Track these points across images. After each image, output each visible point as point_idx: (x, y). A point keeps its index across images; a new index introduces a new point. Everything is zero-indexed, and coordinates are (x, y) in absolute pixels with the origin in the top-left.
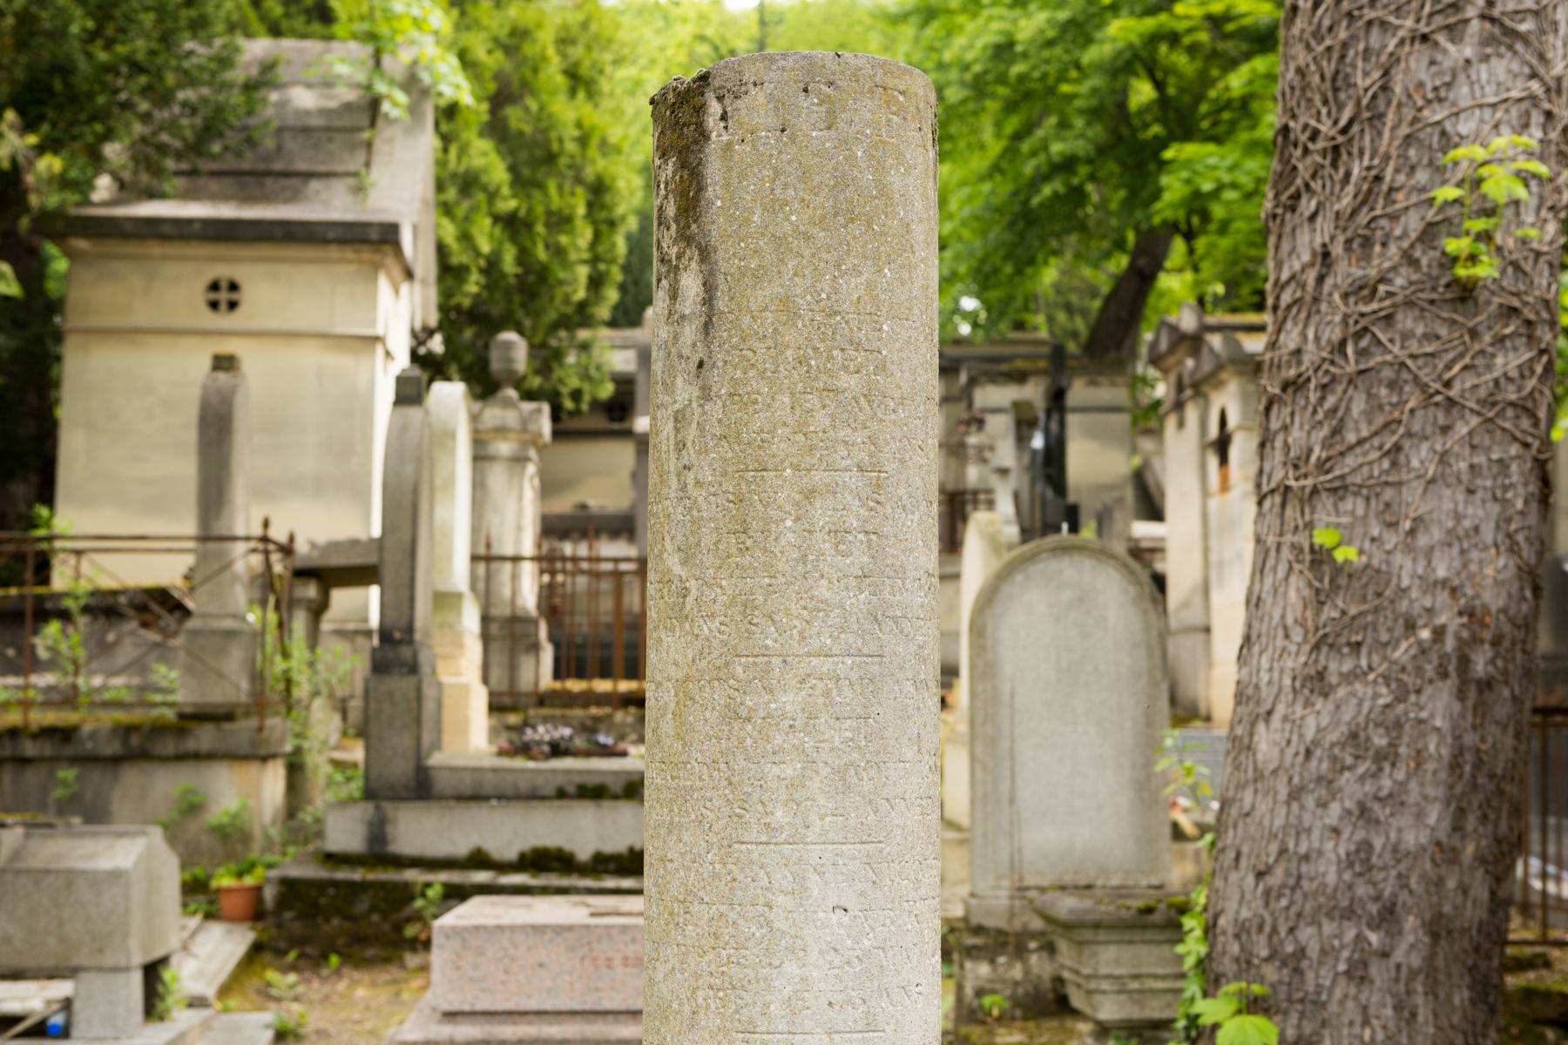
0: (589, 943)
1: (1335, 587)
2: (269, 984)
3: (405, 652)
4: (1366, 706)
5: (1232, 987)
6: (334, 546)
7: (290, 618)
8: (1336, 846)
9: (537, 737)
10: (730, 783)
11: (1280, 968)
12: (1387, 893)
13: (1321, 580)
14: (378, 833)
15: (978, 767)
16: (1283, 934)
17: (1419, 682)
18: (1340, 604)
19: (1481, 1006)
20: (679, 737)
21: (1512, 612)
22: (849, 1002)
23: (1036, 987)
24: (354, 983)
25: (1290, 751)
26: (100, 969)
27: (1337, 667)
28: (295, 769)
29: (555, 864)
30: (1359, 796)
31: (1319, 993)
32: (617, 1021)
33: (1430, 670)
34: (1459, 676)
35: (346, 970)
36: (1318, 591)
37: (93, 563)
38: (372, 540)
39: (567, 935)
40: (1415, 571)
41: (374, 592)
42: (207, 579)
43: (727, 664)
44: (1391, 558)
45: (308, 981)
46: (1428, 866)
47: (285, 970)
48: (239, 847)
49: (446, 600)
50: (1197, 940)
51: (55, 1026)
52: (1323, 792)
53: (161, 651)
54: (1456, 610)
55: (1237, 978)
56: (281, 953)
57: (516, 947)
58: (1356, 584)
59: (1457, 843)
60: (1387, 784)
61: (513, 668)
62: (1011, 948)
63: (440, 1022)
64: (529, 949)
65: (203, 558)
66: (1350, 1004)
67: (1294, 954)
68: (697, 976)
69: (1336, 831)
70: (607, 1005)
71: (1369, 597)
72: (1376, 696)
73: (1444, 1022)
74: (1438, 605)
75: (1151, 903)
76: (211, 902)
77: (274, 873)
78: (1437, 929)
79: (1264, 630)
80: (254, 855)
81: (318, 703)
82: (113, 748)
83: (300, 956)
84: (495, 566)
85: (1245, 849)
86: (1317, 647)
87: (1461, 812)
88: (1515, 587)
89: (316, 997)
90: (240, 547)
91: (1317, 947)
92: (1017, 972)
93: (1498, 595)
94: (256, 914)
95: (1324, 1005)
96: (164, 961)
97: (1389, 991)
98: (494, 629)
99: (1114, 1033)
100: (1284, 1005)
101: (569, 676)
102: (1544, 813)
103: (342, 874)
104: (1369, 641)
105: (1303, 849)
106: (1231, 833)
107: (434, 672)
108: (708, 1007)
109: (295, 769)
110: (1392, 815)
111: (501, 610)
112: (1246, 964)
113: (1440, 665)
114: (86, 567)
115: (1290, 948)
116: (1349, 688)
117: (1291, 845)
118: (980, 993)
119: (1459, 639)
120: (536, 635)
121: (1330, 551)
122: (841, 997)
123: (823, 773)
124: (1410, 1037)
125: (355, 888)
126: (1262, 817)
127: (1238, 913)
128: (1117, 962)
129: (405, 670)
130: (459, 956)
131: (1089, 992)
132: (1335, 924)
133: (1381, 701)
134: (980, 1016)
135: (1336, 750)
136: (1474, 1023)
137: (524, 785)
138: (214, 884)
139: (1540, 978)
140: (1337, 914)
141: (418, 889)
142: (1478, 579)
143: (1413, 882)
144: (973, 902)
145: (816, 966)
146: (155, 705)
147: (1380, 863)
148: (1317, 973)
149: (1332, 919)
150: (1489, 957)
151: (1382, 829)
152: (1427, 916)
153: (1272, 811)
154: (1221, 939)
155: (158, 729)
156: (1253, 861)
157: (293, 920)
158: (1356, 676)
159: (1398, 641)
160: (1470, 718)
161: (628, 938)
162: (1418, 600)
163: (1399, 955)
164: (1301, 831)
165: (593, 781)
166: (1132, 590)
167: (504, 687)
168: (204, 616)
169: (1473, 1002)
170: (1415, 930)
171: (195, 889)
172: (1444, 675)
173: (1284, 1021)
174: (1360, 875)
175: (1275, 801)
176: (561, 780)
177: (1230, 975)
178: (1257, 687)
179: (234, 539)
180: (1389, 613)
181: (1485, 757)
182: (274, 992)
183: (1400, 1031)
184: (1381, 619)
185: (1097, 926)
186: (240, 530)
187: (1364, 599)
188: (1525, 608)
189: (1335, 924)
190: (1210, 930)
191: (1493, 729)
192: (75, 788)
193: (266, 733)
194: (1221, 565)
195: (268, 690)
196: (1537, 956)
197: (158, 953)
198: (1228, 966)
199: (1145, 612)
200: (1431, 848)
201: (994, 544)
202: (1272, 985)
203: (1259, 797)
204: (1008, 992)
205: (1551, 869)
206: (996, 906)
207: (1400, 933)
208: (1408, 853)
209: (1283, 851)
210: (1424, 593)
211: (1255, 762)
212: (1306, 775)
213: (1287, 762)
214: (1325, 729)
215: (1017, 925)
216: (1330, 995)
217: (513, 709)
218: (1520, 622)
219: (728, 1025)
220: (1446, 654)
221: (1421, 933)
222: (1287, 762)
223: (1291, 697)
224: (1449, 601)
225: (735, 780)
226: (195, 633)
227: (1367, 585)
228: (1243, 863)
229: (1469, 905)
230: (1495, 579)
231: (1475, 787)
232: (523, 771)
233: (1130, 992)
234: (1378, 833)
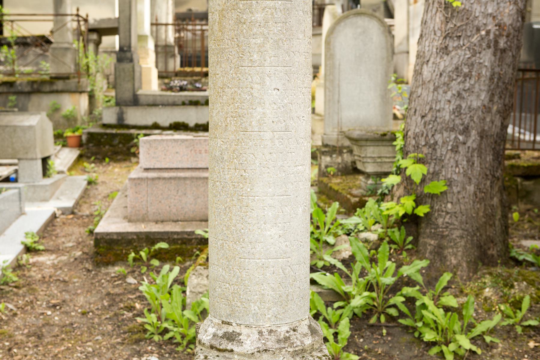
0: (193, 145)
1: (452, 16)
2: (85, 167)
3: (128, 55)
4: (462, 58)
5: (412, 155)
6: (102, 21)
7: (88, 45)
8: (449, 106)
9: (175, 85)
10: (238, 46)
11: (428, 149)
12: (466, 123)
13: (448, 14)
14: (121, 117)
15: (327, 90)
16: (430, 137)
17: (480, 49)
18: (454, 22)
19: (496, 161)
20: (220, 31)
21: (514, 26)
22: (279, 121)
23: (346, 165)
24: (114, 167)
25: (435, 74)
26: (27, 159)
27: (452, 44)
28: (92, 97)
29: (182, 128)
30: (458, 89)
31: (441, 157)
32: (203, 171)
33: (484, 45)
34: (494, 47)
35: (111, 163)
36: (446, 18)
37: (18, 25)
38: (116, 19)
39: (186, 142)
40: (481, 10)
41: (117, 37)
42: (58, 30)
43: (237, 4)
44: (473, 6)
45: (99, 167)
46: (480, 113)
47: (91, 163)
48: (73, 123)
49: (142, 38)
50: (401, 140)
51: (13, 178)
52: (445, 88)
53: (43, 56)
54: (494, 24)
55: (414, 152)
56: (89, 158)
57: (168, 147)
58: (460, 15)
59: (491, 106)
60: (467, 85)
61: (166, 63)
62: (337, 152)
63: (143, 172)
64: (173, 147)
65: (56, 22)
66: (452, 160)
67: (433, 144)
68: (227, 113)
69: (449, 101)
70: (200, 166)
71: (464, 20)
72: (465, 54)
73: (483, 166)
74: (488, 22)
75: (386, 133)
76: (64, 141)
77: (85, 131)
78: (482, 135)
79: (427, 32)
80: (78, 125)
81: (98, 75)
82: (27, 89)
83: (95, 159)
84: (159, 27)
85: (418, 109)
86: (445, 38)
87: (493, 95)
88: (515, 17)
89: (101, 171)
90: (69, 18)
91: (441, 141)
92: (339, 160)
93: (509, 19)
94: (80, 145)
95: (443, 161)
96: (48, 157)
97: (465, 156)
98: (159, 49)
99: (371, 176)
100: (429, 161)
101: (186, 66)
102: (521, 112)
103: (109, 131)
104: (463, 35)
105: (438, 108)
106: (413, 103)
107: (138, 62)
108: (231, 123)
109: (92, 97)
110: (469, 96)
111: (162, 43)
112: (417, 147)
113: (488, 44)
114: (15, 25)
115: (432, 142)
116: (456, 52)
117: (434, 107)
118: (327, 167)
119: (495, 34)
120: (174, 51)
121: (451, 3)
122: (277, 119)
123: (271, 42)
124: (472, 171)
125: (114, 136)
126: (424, 97)
127: (415, 130)
128: (373, 152)
129: (128, 61)
130: (148, 149)
131: (364, 163)
132: (448, 133)
133: (467, 56)
134: (327, 174)
135: (451, 74)
136: (493, 167)
137: (171, 100)
138: (65, 135)
139: (516, 162)
140: (448, 130)
141: (135, 136)
142: (502, 14)
143: (475, 119)
144: (325, 136)
145: (268, 109)
146: (42, 75)
147: (464, 112)
148: (441, 150)
149: (447, 131)
150: (499, 145)
151: (465, 100)
152: (479, 130)
153: (428, 95)
154: (409, 139)
155: (43, 82)
156: (421, 112)
157: (93, 146)
158: (459, 48)
159: (474, 35)
160: (497, 62)
161: (207, 143)
162: (481, 20)
163: (469, 144)
164: (438, 101)
165: (195, 99)
166: (382, 29)
167: (163, 70)
168: (57, 43)
169: (493, 160)
170: (475, 135)
171: (58, 137)
172: (489, 47)
173: (429, 166)
174: (457, 116)
175: (429, 92)
176: (183, 99)
177: (412, 151)
178: (424, 52)
179: (67, 15)
180: (471, 25)
181: (502, 76)
182: (87, 170)
183: (468, 169)
184: (468, 27)
185: (367, 140)
186: (69, 12)
187: (462, 20)
188: (518, 24)
189: (448, 133)
190: (405, 137)
191: (505, 66)
192: (15, 103)
193: (81, 83)
194: (413, 29)
195: (81, 70)
196: (516, 155)
197: (46, 155)
198: (411, 148)
199: (386, 37)
200: (482, 107)
201: (334, 15)
202: (426, 154)
203: (424, 90)
204: (336, 167)
205: (522, 131)
206: (333, 138)
207: (470, 136)
208: (474, 109)
209: (431, 109)
210: (484, 18)
211: (422, 79)
212: (440, 82)
213: (434, 78)
214: (447, 66)
215: (340, 144)
216: (445, 157)
217: (166, 77)
218: (516, 29)
219: (238, 129)
220: (490, 40)
221: (477, 136)
222: (434, 78)
223: (436, 55)
224: (492, 21)
225: (240, 45)
226: (55, 49)
227: (464, 15)
228: (417, 113)
229: (494, 127)
230: (509, 13)
231: (498, 86)
232: (170, 96)
233: (378, 162)
234: (464, 102)
